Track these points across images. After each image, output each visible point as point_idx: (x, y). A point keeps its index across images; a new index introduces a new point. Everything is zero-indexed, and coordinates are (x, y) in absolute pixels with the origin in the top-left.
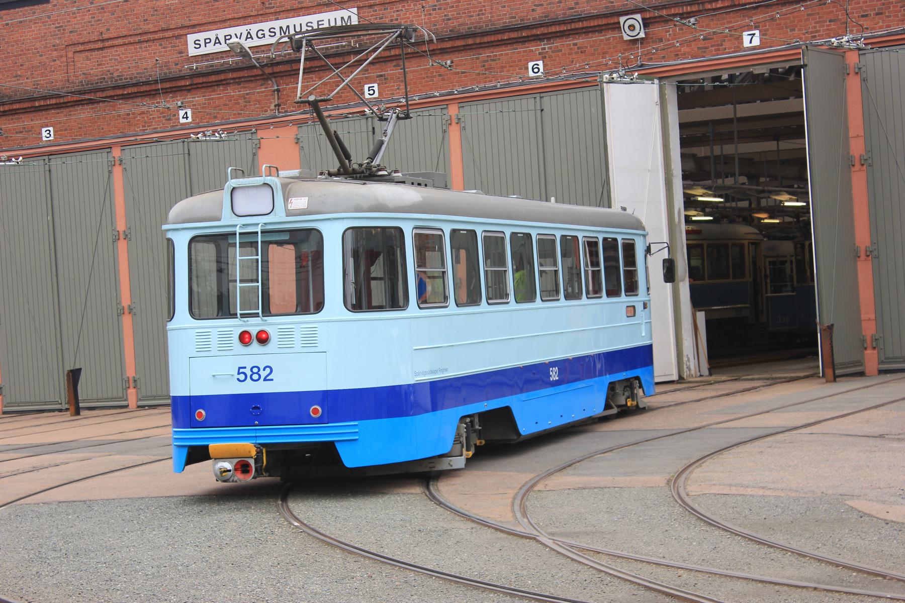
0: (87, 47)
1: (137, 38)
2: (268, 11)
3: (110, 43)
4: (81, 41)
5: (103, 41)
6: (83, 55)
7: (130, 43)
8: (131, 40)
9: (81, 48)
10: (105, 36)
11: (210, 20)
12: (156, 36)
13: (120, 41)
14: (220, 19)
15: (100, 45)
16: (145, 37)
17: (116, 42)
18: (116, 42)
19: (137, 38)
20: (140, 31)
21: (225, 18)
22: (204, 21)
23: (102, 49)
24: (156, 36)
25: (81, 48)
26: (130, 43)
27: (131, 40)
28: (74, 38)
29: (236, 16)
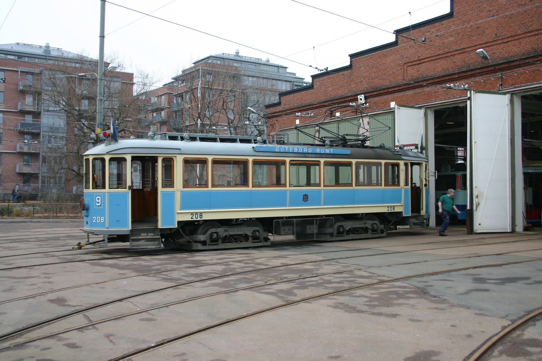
0: (413, 64)
1: (435, 58)
2: (498, 39)
3: (423, 61)
4: (410, 61)
5: (419, 60)
6: (411, 67)
7: (432, 60)
8: (432, 59)
9: (410, 64)
10: (421, 58)
11: (469, 46)
12: (443, 56)
13: (427, 60)
14: (474, 45)
15: (418, 62)
16: (438, 57)
17: (425, 60)
18: (425, 60)
19: (435, 58)
20: (436, 54)
21: (476, 44)
22: (466, 47)
23: (419, 64)
24: (443, 56)
25: (410, 64)
26: (432, 60)
27: (432, 59)
28: (407, 60)
29: (482, 42)
